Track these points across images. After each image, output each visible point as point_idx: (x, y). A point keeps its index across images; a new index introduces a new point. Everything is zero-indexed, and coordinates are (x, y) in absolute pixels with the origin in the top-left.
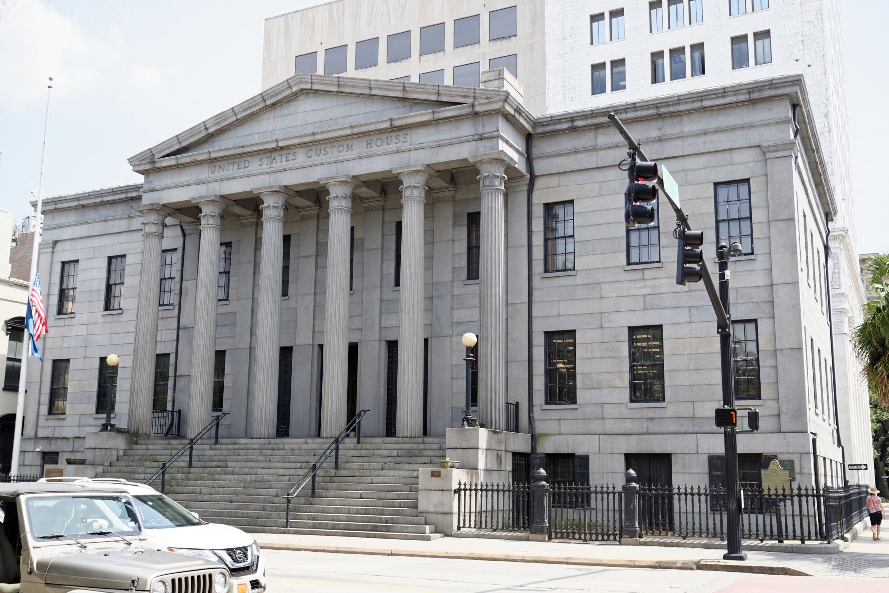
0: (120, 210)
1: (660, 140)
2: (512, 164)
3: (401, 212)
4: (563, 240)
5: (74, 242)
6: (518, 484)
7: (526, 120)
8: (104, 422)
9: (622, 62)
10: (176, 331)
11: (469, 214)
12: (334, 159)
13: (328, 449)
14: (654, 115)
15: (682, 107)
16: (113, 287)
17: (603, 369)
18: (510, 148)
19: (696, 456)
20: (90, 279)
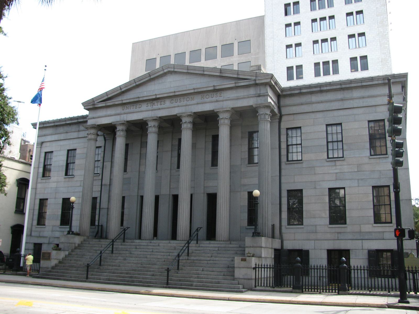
0: (74, 128)
1: (342, 100)
2: (273, 108)
3: (219, 130)
4: (332, 144)
5: (52, 143)
6: (330, 265)
7: (279, 88)
8: (68, 230)
9: (301, 66)
10: (100, 186)
11: (249, 132)
12: (185, 104)
13: (184, 246)
14: (339, 88)
15: (353, 85)
16: (69, 164)
17: (316, 208)
18: (271, 100)
19: (361, 250)
20: (59, 160)
